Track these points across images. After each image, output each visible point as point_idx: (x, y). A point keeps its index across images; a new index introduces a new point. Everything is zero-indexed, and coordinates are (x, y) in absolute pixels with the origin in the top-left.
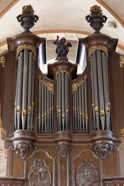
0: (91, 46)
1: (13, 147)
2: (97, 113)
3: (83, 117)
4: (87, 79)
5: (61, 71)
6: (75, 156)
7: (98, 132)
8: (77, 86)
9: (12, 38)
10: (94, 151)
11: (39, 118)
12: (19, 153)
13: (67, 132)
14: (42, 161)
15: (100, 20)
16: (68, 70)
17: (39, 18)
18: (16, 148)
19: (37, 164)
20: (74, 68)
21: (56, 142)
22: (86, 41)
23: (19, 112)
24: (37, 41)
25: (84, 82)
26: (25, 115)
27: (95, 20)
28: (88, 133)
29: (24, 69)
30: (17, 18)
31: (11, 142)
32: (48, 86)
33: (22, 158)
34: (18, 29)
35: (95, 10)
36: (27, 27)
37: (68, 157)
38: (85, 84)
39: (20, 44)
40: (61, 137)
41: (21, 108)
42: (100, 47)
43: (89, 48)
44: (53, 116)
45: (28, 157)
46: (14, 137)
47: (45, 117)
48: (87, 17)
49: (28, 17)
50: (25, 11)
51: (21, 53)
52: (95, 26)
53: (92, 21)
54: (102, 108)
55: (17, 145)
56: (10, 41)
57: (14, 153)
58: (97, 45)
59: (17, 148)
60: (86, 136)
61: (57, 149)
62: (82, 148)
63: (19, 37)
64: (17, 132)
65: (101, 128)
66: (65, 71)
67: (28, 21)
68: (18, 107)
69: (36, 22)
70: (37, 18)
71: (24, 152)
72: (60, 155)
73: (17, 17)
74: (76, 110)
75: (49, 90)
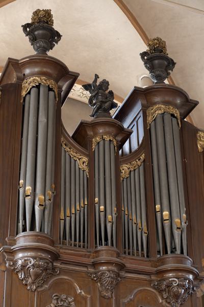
0: (155, 104)
1: (13, 264)
2: (167, 223)
3: (139, 225)
4: (144, 161)
5: (105, 136)
6: (126, 297)
7: (169, 258)
8: (128, 169)
9: (18, 61)
10: (160, 291)
11: (62, 217)
12: (24, 278)
13: (114, 248)
14: (66, 299)
15: (166, 63)
16: (115, 136)
17: (176, 65)
18: (22, 266)
19: (58, 303)
20: (125, 135)
21: (95, 265)
22: (145, 94)
23: (30, 197)
24: (63, 74)
25: (141, 165)
26: (43, 205)
27: (156, 62)
28: (148, 256)
29: (40, 120)
30: (175, 62)
31: (10, 253)
32: (79, 159)
33: (30, 288)
34: (24, 49)
35: (158, 45)
36: (44, 47)
37: (113, 296)
38: (141, 168)
39: (32, 75)
40: (104, 257)
41: (33, 191)
42: (172, 108)
43: (149, 107)
44: (86, 217)
45: (41, 286)
46: (15, 244)
47: (73, 216)
48: (25, 27)
49: (42, 30)
50: (39, 19)
51: (34, 89)
52: (158, 73)
53: (152, 64)
54: (173, 215)
55: (25, 260)
56: (13, 64)
57: (14, 276)
58: (166, 103)
59: (23, 266)
60: (146, 261)
61: (95, 279)
62: (139, 282)
63: (31, 61)
64: (24, 236)
65: (173, 250)
66: (111, 139)
67: (43, 37)
68: (29, 188)
69: (57, 43)
70: (59, 36)
71: (37, 276)
72: (100, 292)
73: (22, 26)
74: (126, 213)
75: (80, 167)
